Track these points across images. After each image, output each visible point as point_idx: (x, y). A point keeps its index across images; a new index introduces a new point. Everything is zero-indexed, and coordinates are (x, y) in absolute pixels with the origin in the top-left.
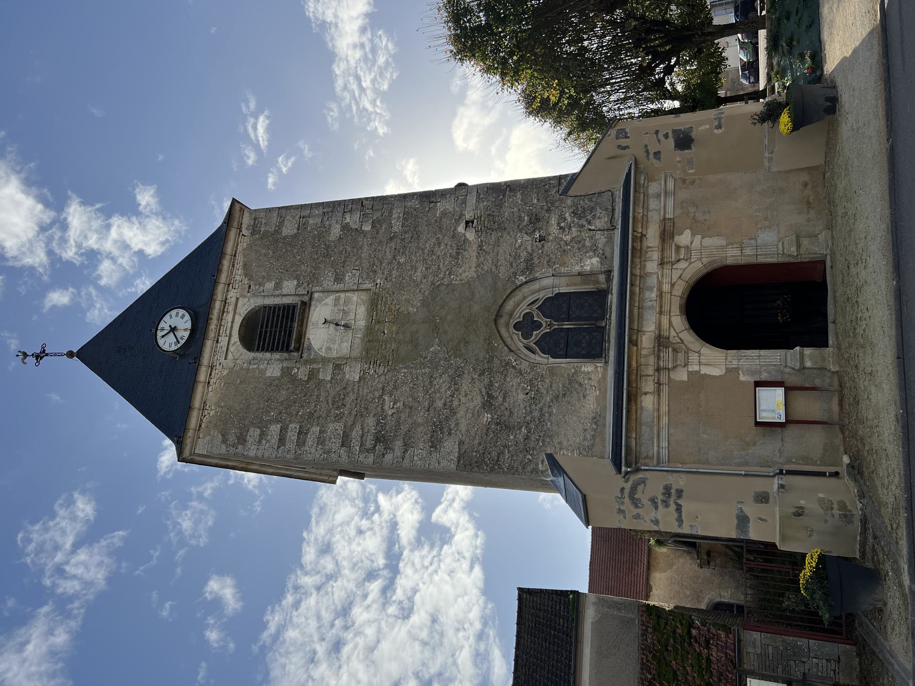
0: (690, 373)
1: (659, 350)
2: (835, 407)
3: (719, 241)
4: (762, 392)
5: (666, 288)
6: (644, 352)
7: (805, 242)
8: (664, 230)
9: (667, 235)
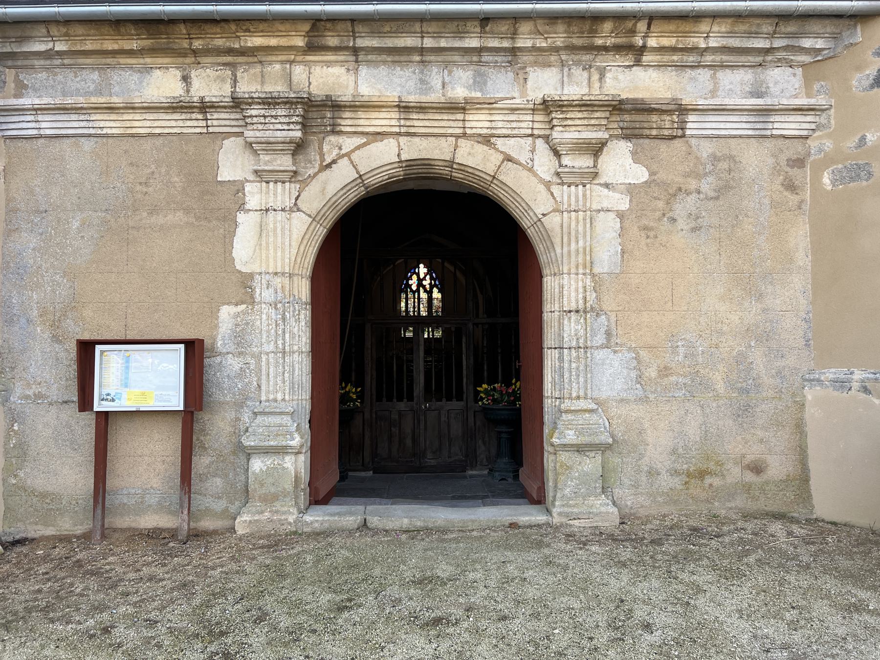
0: (238, 188)
2: (149, 521)
3: (606, 256)
4: (171, 362)
5: (478, 122)
6: (299, 72)
7: (590, 464)
8: (651, 111)
9: (633, 118)
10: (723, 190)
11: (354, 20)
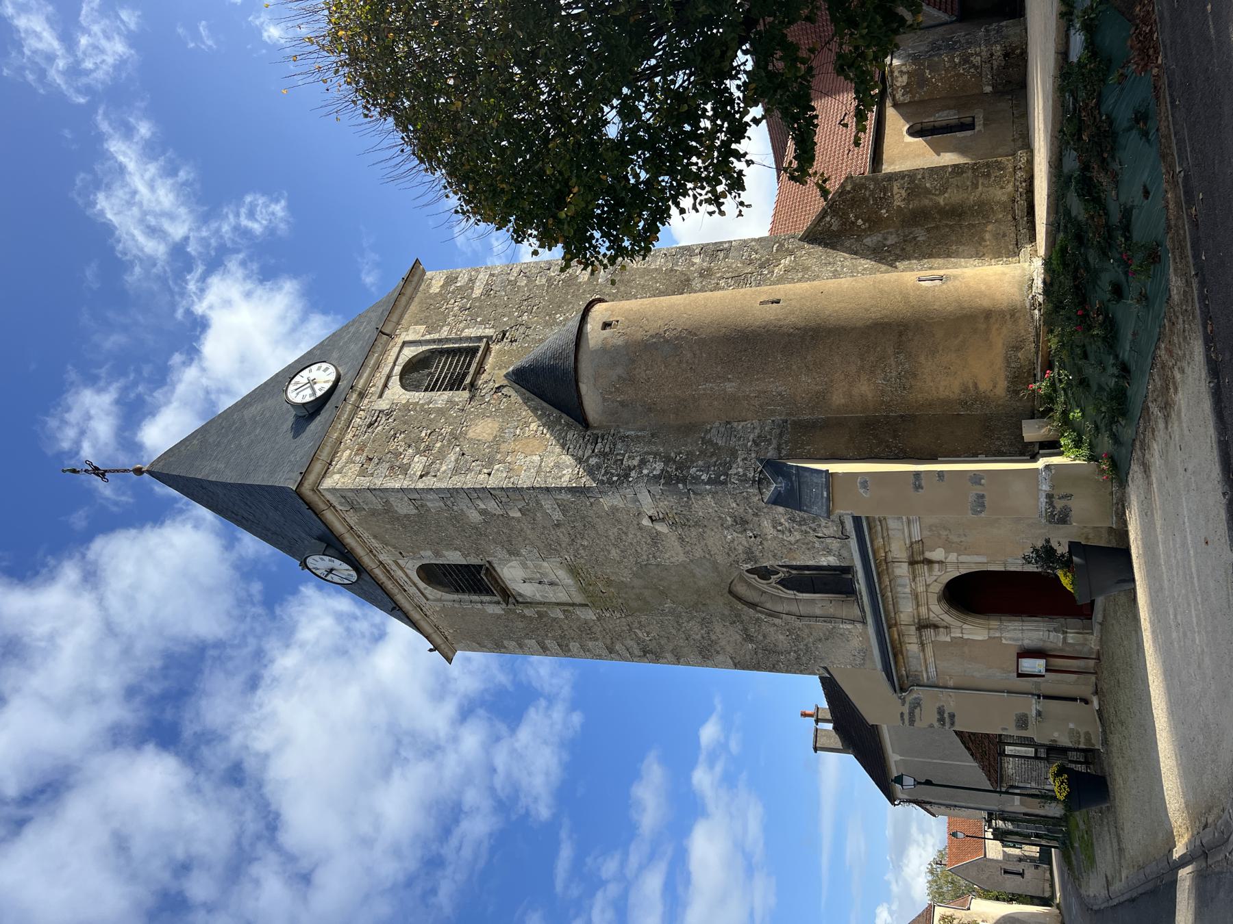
1: (921, 636)
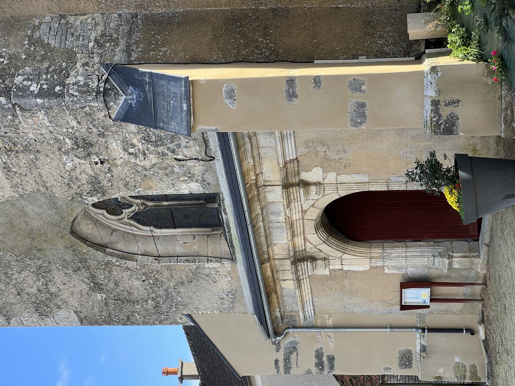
0: (330, 271)
10: (323, 144)
11: (256, 245)
